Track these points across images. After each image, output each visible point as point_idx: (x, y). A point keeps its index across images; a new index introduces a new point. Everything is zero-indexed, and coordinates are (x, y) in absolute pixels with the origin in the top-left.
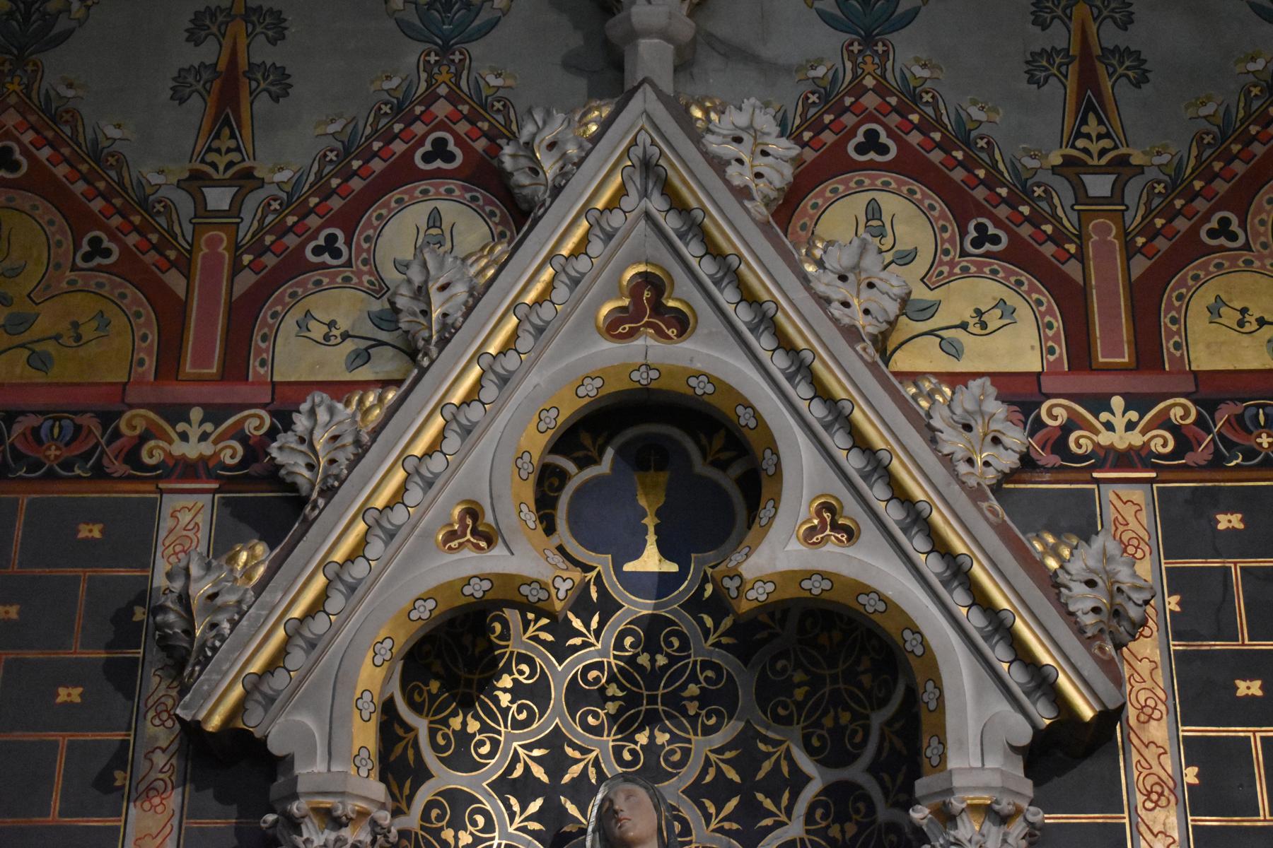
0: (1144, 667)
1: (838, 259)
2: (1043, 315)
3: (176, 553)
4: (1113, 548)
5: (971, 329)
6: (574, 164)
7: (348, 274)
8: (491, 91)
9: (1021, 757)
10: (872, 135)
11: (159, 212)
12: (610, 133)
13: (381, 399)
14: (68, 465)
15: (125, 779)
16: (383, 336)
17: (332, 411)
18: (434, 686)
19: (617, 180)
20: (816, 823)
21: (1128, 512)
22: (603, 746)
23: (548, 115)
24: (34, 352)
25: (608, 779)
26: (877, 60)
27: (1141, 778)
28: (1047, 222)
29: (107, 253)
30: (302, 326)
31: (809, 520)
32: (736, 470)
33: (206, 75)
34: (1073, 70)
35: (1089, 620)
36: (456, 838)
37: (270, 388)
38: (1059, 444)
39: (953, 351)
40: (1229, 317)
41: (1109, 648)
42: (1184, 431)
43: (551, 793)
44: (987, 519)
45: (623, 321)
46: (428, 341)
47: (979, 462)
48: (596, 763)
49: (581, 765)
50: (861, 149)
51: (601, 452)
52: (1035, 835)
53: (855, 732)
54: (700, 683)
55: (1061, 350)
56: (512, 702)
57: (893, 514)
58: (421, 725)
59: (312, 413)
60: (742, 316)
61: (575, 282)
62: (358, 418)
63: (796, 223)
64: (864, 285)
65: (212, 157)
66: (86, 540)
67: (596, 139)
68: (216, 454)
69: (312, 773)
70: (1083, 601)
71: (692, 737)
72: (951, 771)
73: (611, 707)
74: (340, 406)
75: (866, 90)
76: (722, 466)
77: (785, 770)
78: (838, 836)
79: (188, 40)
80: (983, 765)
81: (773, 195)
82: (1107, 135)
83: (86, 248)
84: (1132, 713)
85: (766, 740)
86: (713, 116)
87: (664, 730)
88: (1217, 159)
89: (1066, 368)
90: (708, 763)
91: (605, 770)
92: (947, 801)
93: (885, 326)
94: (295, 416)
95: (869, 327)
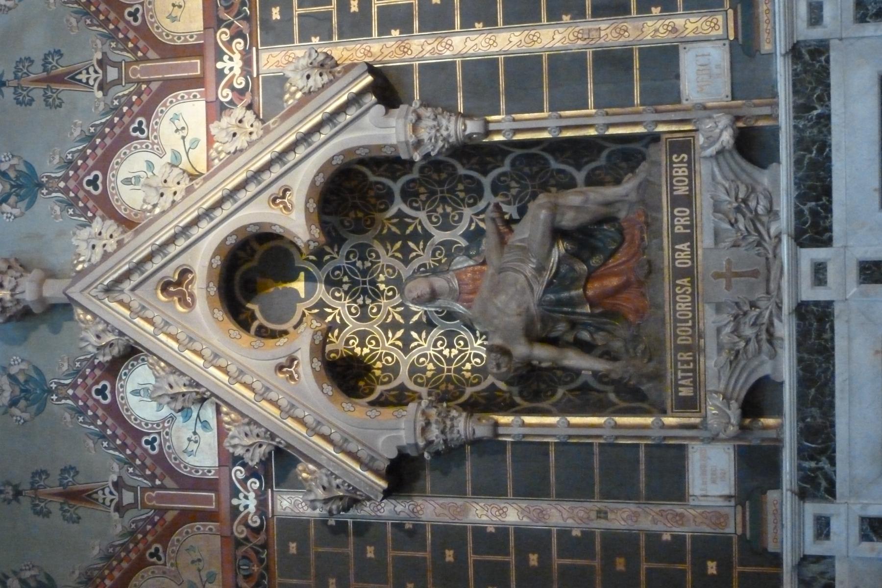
0: (346, 54)
1: (154, 198)
2: (177, 100)
3: (303, 507)
4: (291, 67)
5: (185, 135)
6: (107, 326)
7: (164, 433)
8: (70, 368)
10: (89, 183)
11: (136, 526)
12: (90, 308)
13: (227, 414)
14: (261, 561)
16: (195, 415)
17: (233, 437)
18: (361, 384)
19: (115, 305)
21: (272, 60)
23: (82, 339)
24: (207, 581)
26: (51, 181)
28: (131, 98)
29: (157, 550)
30: (190, 454)
31: (281, 209)
32: (255, 245)
33: (66, 508)
34: (55, 86)
35: (326, 78)
36: (431, 370)
37: (222, 468)
38: (241, 92)
39: (196, 143)
40: (177, 12)
41: (339, 69)
42: (233, 34)
43: (408, 328)
44: (278, 126)
45: (185, 300)
46: (197, 393)
47: (251, 129)
48: (394, 307)
50: (96, 188)
51: (249, 309)
55: (194, 91)
56: (367, 347)
57: (277, 170)
58: (379, 389)
59: (235, 446)
60: (182, 243)
61: (167, 323)
62: (237, 424)
63: (134, 218)
64: (165, 185)
65: (107, 503)
66: (366, 550)
67: (95, 316)
68: (254, 491)
69: (406, 437)
70: (317, 81)
71: (381, 264)
73: (368, 301)
74: (231, 433)
75: (66, 186)
76: (254, 251)
79: (48, 517)
81: (121, 229)
82: (87, 69)
83: (155, 559)
84: (367, 60)
86: (81, 259)
87: (378, 277)
88: (98, 17)
89: (203, 89)
90: (393, 256)
93: (185, 175)
94: (237, 454)
95: (186, 183)
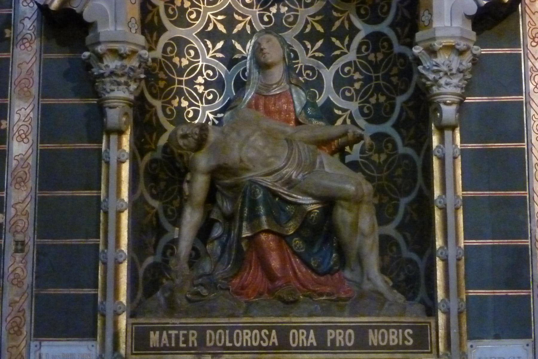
9: (470, 20)
15: (11, 33)
20: (362, 53)
22: (253, 14)
25: (257, 32)
27: (530, 30)
36: (181, 62)
48: (250, 23)
49: (243, 24)
52: (476, 60)
53: (383, 7)
54: (354, 89)
69: (107, 31)
71: (299, 8)
72: (435, 29)
77: (347, 26)
78: (374, 59)
80: (451, 25)
85: (337, 10)
87: (285, 5)
90: (307, 22)
91: (255, 26)
92: (433, 44)
